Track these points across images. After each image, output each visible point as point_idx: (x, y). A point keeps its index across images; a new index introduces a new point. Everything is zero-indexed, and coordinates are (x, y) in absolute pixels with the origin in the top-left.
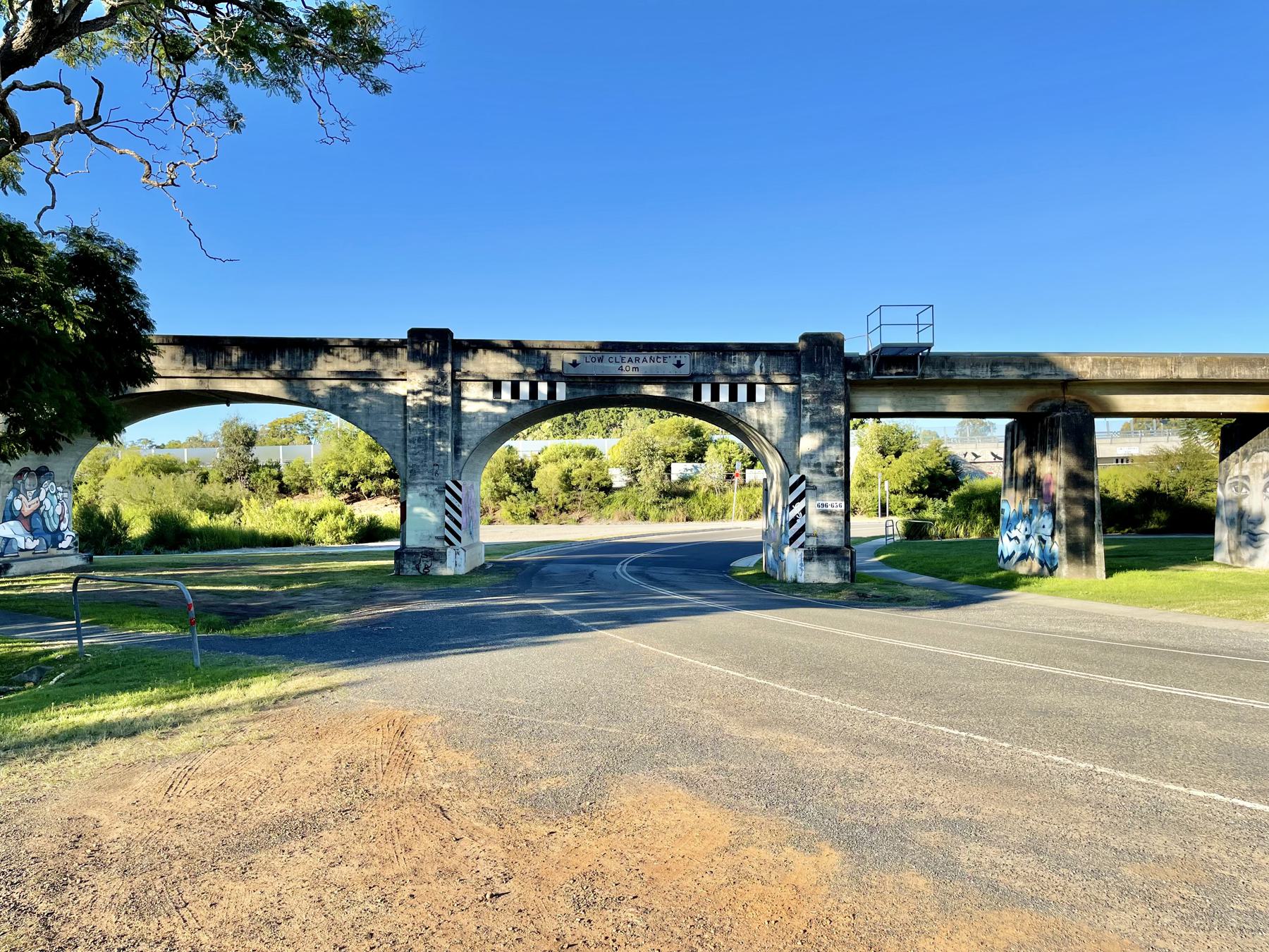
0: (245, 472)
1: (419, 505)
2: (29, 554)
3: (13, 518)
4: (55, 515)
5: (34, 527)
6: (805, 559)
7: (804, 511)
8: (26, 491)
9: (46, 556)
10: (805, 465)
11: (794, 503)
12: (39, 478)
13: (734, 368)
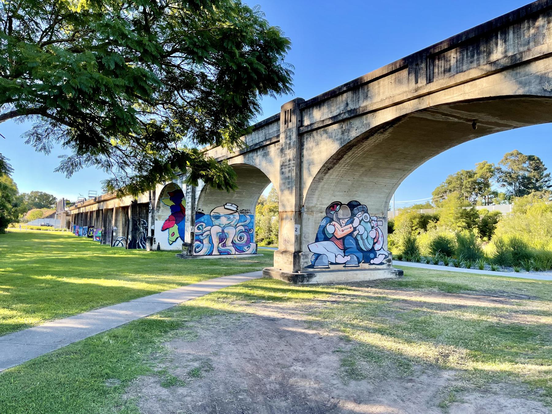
2: (341, 267)
3: (326, 239)
4: (369, 238)
8: (339, 219)
9: (357, 268)
12: (352, 210)
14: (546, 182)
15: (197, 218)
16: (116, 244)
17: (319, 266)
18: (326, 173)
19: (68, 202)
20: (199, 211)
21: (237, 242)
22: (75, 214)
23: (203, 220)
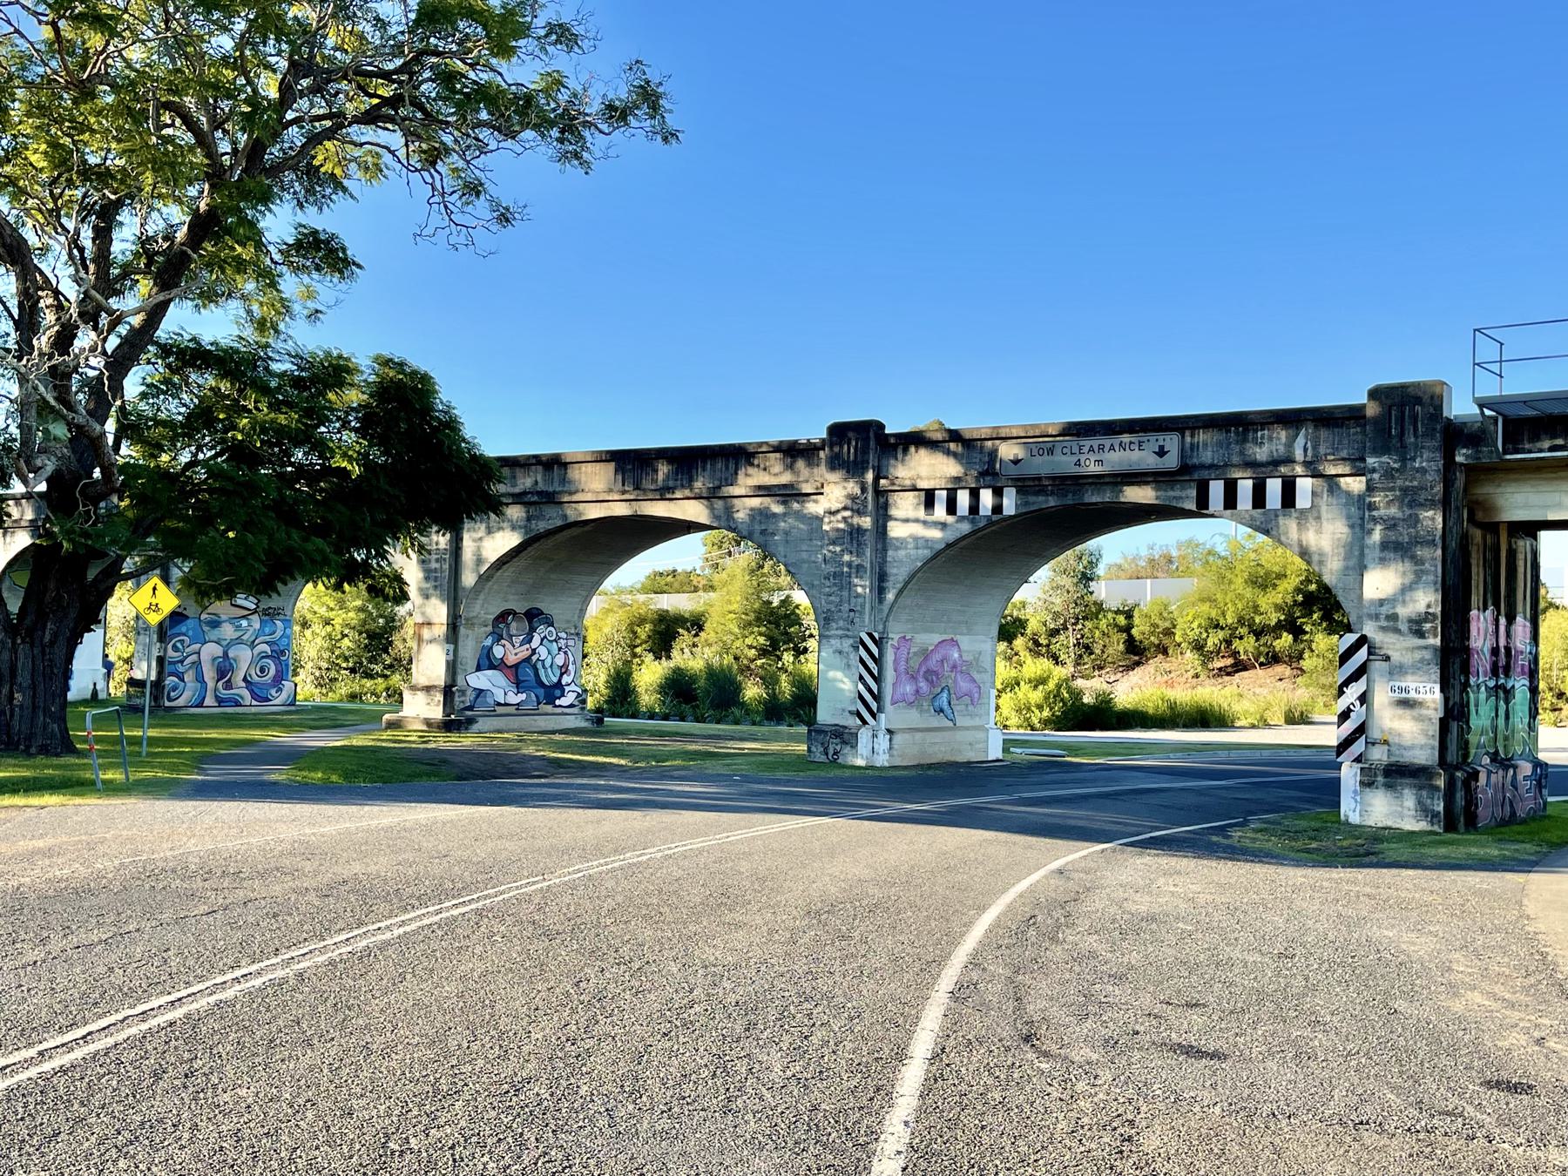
0: (1078, 619)
1: (836, 669)
2: (512, 710)
3: (492, 667)
4: (555, 667)
6: (1362, 783)
7: (1363, 698)
8: (511, 636)
9: (535, 713)
10: (1370, 617)
11: (1346, 683)
12: (530, 622)
13: (1261, 453)
18: (498, 569)
23: (184, 629)
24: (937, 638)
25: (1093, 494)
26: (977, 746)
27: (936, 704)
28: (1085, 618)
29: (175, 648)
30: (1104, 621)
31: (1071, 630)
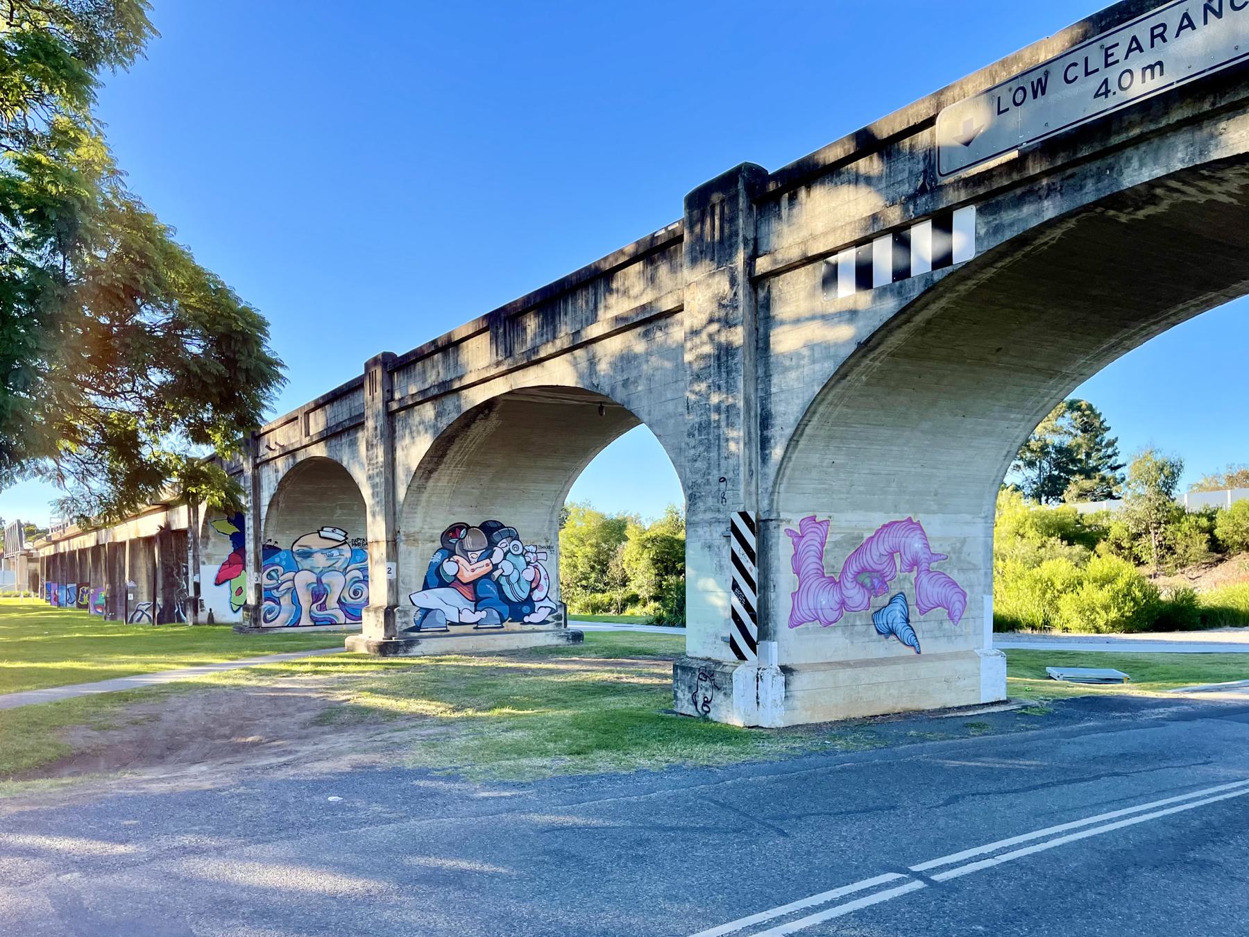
0: (1160, 523)
2: (470, 629)
3: (443, 584)
4: (522, 581)
5: (481, 596)
9: (499, 630)
12: (489, 536)
14: (1110, 457)
15: (265, 558)
16: (136, 618)
17: (428, 627)
18: (428, 479)
19: (31, 528)
20: (269, 543)
21: (350, 600)
22: (48, 557)
23: (277, 560)
24: (879, 519)
25: (1141, 166)
26: (961, 683)
27: (881, 622)
28: (1167, 522)
29: (269, 576)
30: (1186, 524)
31: (1153, 533)
